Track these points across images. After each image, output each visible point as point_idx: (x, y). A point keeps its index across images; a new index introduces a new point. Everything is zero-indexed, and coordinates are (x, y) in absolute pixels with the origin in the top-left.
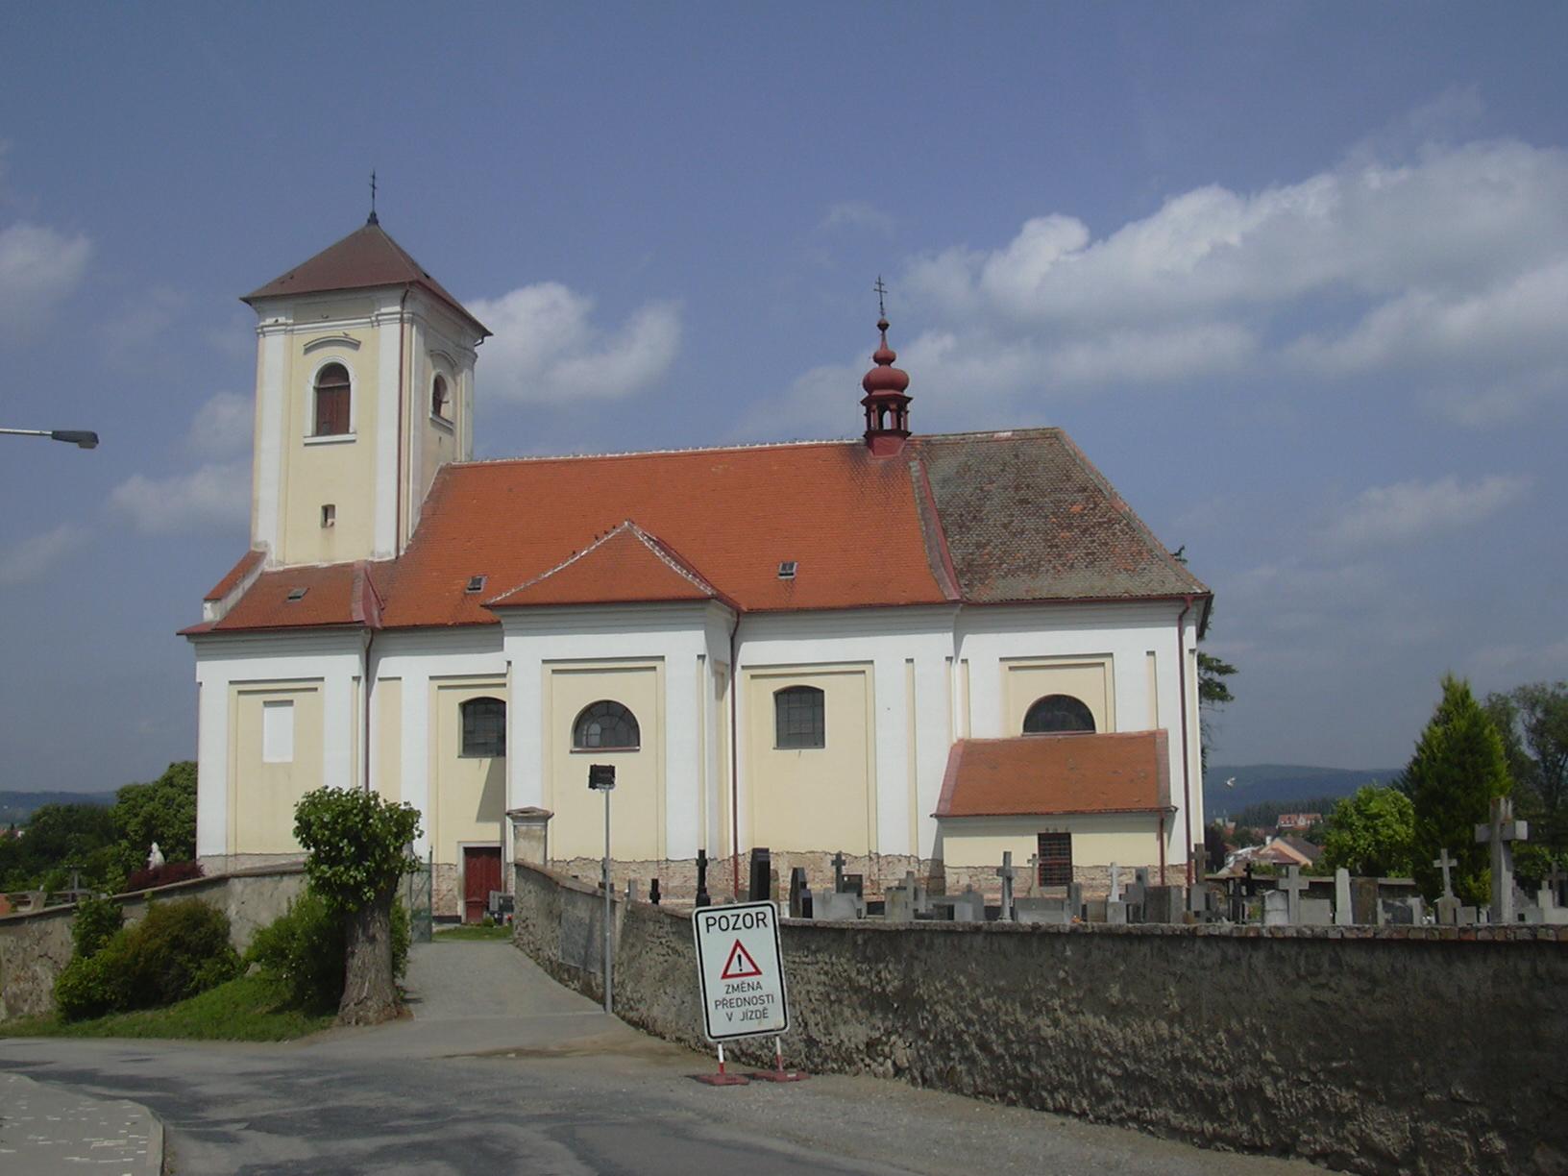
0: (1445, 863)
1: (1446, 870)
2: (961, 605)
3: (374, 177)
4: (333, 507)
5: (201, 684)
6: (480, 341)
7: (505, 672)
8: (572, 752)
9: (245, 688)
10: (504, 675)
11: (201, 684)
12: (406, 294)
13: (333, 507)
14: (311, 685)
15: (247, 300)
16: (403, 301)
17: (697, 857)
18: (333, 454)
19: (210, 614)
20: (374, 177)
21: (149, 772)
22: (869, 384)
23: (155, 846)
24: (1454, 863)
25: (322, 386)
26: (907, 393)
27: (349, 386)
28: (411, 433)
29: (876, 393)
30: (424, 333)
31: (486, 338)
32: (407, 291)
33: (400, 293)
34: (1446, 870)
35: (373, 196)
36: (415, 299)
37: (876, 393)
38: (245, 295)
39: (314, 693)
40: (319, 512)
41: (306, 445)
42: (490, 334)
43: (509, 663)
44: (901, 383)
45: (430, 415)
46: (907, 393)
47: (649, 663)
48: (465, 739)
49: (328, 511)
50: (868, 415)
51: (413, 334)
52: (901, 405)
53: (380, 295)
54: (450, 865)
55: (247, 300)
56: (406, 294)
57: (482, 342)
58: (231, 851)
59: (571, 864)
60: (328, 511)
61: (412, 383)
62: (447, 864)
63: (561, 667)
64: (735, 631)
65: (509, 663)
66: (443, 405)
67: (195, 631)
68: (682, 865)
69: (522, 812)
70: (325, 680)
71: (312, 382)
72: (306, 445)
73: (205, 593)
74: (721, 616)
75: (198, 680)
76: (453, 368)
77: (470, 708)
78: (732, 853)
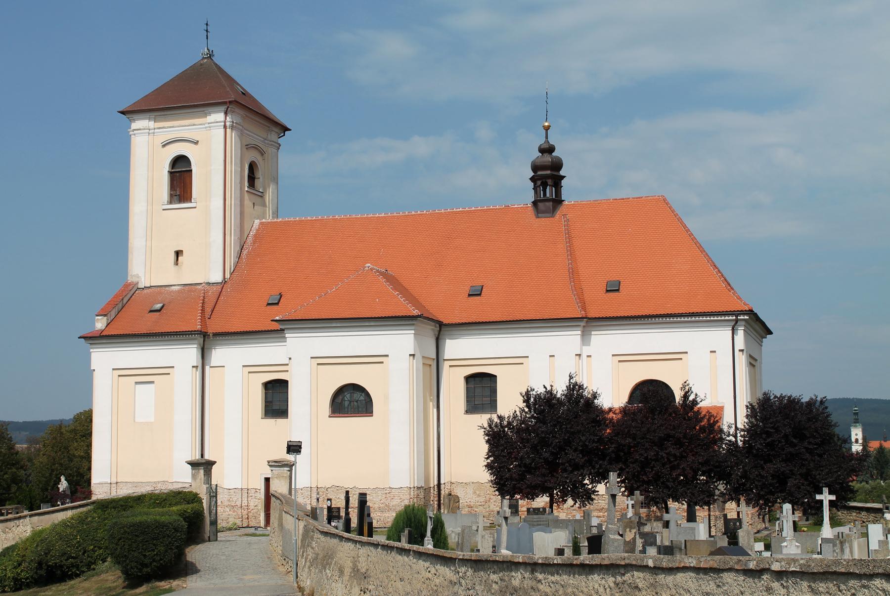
0: (826, 497)
1: (826, 505)
2: (585, 320)
3: (207, 24)
4: (182, 251)
5: (94, 370)
6: (283, 134)
7: (288, 363)
8: (330, 417)
9: (123, 373)
10: (287, 365)
11: (94, 370)
12: (227, 110)
13: (182, 251)
14: (165, 371)
15: (123, 113)
16: (226, 113)
17: (852, 447)
18: (181, 214)
19: (100, 324)
20: (207, 24)
21: (66, 413)
22: (535, 168)
23: (63, 478)
24: (833, 498)
25: (173, 171)
26: (562, 173)
27: (192, 170)
28: (232, 201)
29: (539, 173)
30: (241, 135)
31: (286, 132)
32: (228, 107)
33: (224, 108)
34: (826, 505)
35: (207, 38)
36: (234, 112)
37: (539, 173)
38: (121, 110)
39: (168, 375)
40: (172, 256)
41: (164, 210)
42: (290, 130)
43: (290, 359)
44: (557, 165)
45: (246, 189)
46: (562, 173)
47: (378, 359)
48: (266, 406)
49: (178, 253)
50: (535, 189)
51: (232, 136)
52: (557, 181)
53: (210, 109)
54: (256, 489)
55: (123, 113)
56: (227, 110)
57: (284, 135)
58: (114, 480)
59: (329, 489)
60: (178, 253)
61: (232, 168)
62: (253, 489)
63: (322, 361)
64: (439, 335)
65: (290, 359)
66: (256, 180)
67: (89, 335)
68: (399, 491)
69: (275, 462)
70: (155, 382)
71: (166, 168)
72: (164, 210)
73: (97, 311)
74: (429, 330)
75: (92, 368)
76: (262, 155)
77: (269, 385)
78: (436, 483)
